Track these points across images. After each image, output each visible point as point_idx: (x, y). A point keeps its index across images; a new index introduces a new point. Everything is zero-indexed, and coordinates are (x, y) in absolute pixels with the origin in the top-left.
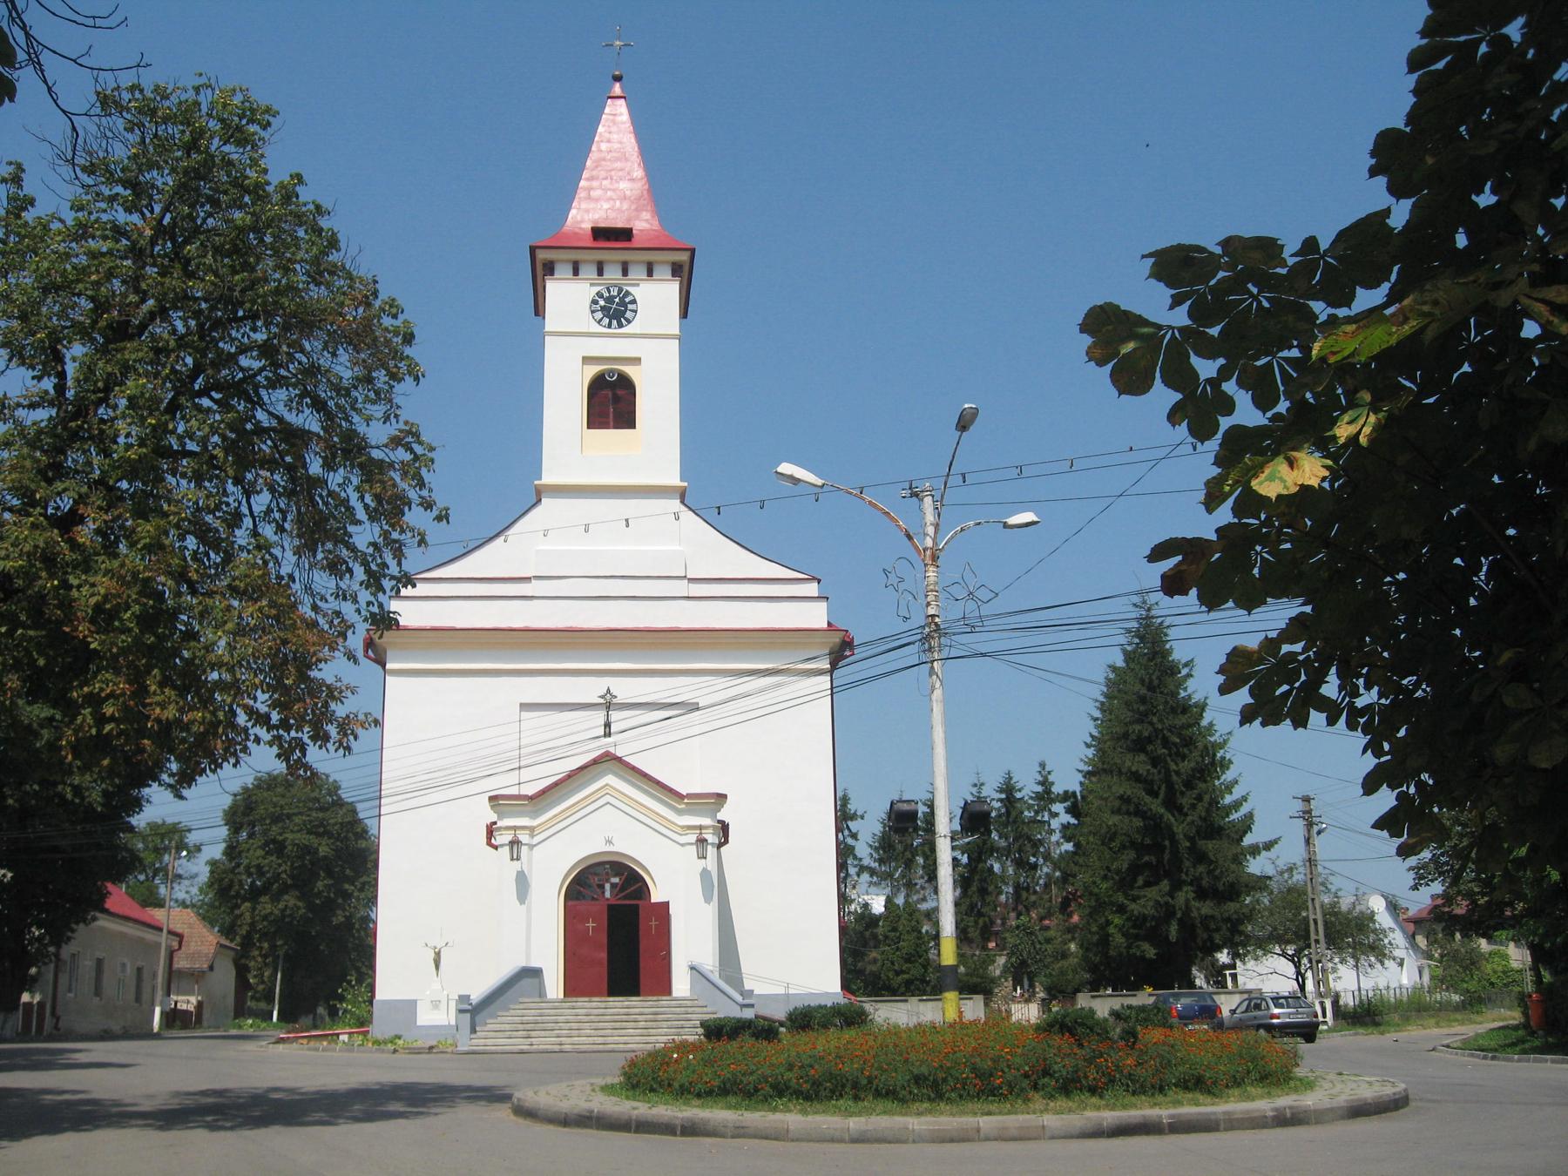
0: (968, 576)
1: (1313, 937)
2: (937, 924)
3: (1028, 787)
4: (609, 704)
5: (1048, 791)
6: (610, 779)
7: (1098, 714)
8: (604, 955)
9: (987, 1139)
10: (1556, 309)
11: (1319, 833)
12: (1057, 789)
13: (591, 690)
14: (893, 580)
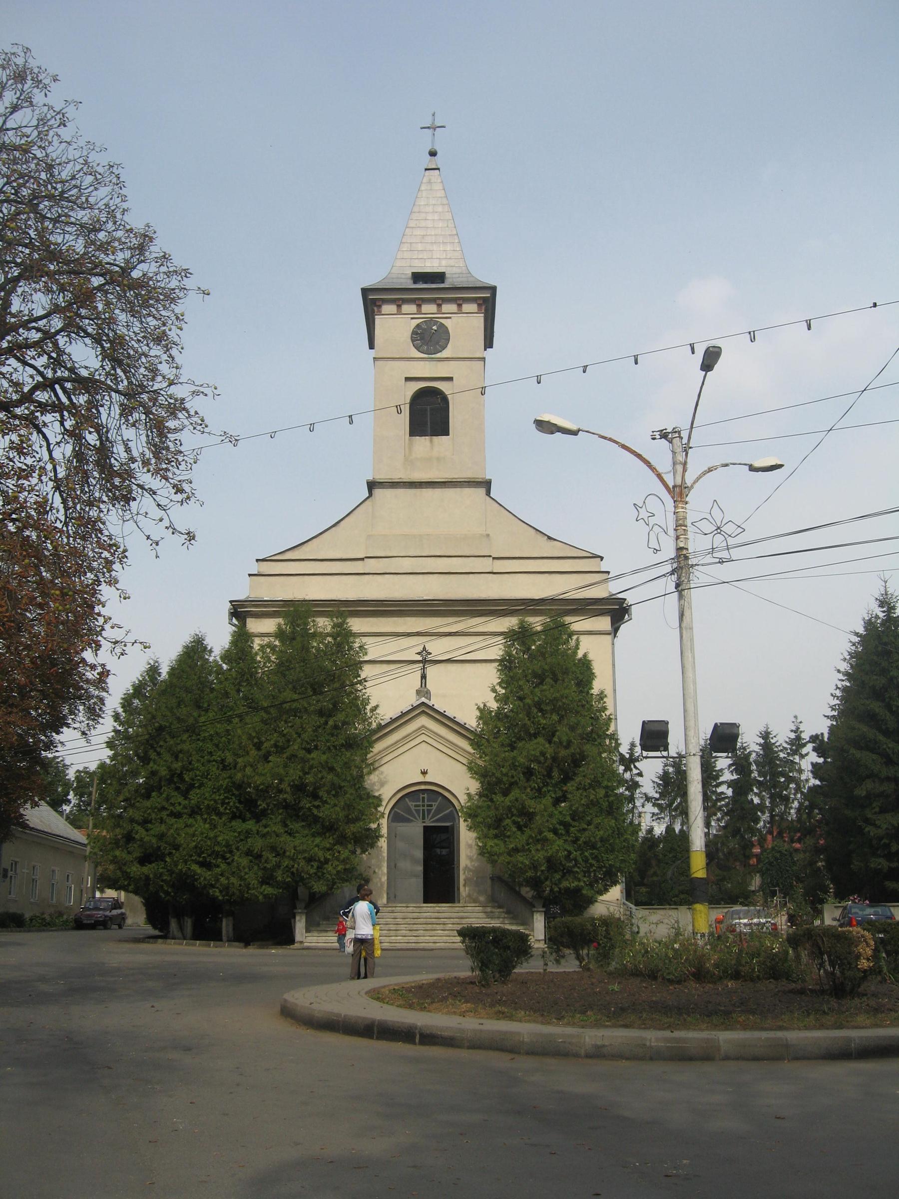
3: (782, 737)
4: (425, 661)
5: (798, 738)
6: (423, 721)
7: (838, 693)
8: (420, 868)
9: (727, 1058)
12: (806, 736)
13: (409, 649)
14: (643, 514)
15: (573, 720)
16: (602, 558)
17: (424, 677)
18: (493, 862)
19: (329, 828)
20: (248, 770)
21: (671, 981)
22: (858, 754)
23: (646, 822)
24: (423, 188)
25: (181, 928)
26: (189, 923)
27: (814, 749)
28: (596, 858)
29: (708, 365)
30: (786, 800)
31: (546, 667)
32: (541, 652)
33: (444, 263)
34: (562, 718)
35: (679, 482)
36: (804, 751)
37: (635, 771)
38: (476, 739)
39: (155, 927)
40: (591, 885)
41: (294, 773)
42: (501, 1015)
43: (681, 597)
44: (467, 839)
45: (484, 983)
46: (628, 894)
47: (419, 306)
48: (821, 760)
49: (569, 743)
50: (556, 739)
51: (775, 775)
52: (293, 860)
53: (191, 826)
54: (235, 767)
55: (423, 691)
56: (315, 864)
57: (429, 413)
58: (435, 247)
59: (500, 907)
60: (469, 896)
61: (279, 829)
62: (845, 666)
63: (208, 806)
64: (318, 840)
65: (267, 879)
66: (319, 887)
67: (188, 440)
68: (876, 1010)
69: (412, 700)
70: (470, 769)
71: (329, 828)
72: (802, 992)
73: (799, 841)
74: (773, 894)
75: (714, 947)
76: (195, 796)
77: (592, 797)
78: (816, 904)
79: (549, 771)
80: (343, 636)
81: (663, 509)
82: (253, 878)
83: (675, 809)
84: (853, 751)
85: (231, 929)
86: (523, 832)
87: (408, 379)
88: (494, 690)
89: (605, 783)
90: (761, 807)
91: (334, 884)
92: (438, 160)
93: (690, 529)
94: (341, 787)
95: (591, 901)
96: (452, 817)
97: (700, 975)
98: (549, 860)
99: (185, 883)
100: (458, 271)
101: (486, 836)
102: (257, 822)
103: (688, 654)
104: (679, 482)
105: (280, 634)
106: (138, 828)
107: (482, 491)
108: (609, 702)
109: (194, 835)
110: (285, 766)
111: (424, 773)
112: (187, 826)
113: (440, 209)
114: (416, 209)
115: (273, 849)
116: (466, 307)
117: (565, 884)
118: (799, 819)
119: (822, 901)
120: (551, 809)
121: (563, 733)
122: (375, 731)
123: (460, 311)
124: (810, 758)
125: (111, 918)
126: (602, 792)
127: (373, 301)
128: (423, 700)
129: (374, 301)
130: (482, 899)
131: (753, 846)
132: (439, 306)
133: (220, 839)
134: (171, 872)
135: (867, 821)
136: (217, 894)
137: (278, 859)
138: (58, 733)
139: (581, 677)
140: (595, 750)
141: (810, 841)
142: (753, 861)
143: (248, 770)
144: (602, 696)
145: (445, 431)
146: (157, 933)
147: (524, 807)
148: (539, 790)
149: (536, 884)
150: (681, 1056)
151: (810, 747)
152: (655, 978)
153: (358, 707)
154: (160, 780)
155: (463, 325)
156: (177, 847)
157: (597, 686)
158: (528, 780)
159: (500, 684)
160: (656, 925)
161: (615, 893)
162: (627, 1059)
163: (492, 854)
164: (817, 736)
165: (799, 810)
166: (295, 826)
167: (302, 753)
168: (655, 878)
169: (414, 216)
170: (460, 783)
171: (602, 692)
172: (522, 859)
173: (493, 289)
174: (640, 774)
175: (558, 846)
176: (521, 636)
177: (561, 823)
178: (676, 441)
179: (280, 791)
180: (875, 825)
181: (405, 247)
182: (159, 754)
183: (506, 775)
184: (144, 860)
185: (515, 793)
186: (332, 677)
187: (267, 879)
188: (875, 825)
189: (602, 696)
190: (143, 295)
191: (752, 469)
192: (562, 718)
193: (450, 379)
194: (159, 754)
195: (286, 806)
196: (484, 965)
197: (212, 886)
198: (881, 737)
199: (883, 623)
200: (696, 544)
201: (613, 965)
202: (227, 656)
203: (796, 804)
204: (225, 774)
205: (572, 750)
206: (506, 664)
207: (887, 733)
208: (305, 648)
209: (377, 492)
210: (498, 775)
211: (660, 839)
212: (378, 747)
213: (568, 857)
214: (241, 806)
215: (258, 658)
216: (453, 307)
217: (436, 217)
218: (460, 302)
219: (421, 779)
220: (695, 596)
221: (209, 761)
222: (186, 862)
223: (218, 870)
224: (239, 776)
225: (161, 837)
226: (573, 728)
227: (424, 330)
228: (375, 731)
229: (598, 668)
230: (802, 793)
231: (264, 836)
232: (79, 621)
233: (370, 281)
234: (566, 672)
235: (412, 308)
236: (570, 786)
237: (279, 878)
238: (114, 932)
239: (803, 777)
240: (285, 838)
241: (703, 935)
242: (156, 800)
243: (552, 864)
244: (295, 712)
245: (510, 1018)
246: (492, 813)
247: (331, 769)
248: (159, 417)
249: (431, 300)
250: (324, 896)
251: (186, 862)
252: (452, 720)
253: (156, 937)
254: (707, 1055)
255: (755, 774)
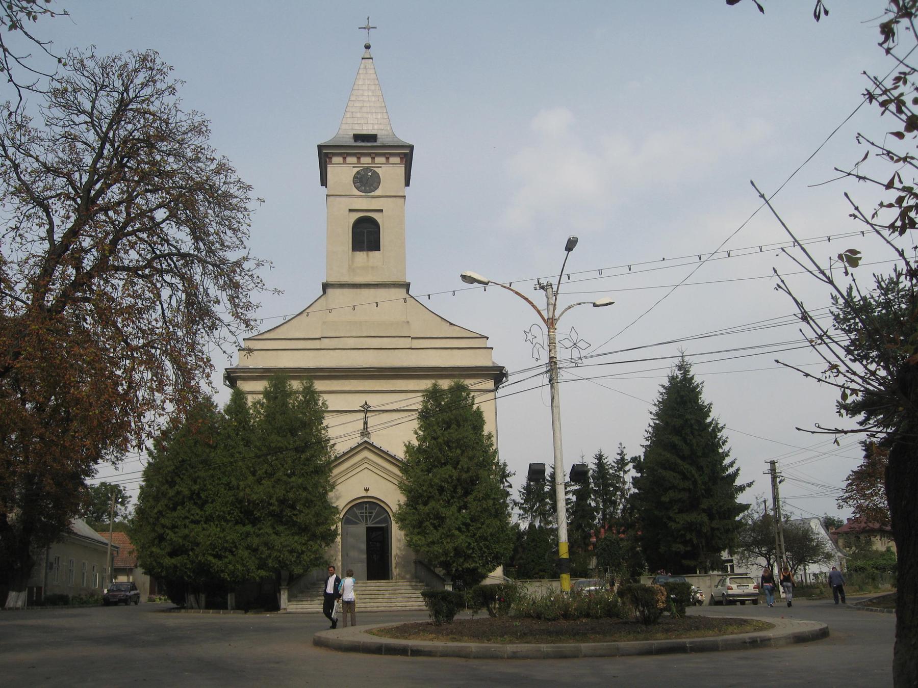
0: (574, 335)
1: (777, 542)
2: (557, 536)
3: (611, 458)
4: (366, 409)
5: (623, 459)
6: (366, 454)
7: (650, 430)
8: (365, 556)
9: (585, 656)
10: (3, 452)
11: (780, 482)
12: (628, 458)
13: (356, 402)
14: (530, 337)
15: (471, 453)
16: (488, 338)
17: (366, 423)
18: (417, 552)
19: (303, 529)
20: (248, 490)
21: (549, 620)
22: (664, 473)
23: (514, 520)
24: (361, 72)
25: (198, 602)
26: (203, 598)
27: (634, 467)
28: (487, 547)
29: (571, 245)
30: (614, 503)
31: (452, 417)
32: (448, 407)
33: (376, 127)
34: (463, 452)
35: (551, 316)
36: (627, 468)
37: (506, 484)
38: (404, 467)
39: (173, 602)
40: (484, 566)
41: (280, 492)
42: (453, 640)
43: (552, 387)
44: (398, 536)
45: (438, 624)
46: (506, 573)
47: (359, 158)
48: (639, 475)
49: (468, 470)
50: (459, 466)
51: (606, 486)
52: (280, 551)
53: (207, 530)
54: (238, 488)
55: (365, 432)
56: (295, 555)
57: (366, 234)
58: (369, 116)
59: (420, 582)
60: (399, 574)
61: (270, 530)
62: (654, 409)
63: (219, 516)
64: (296, 538)
65: (262, 565)
66: (298, 570)
67: (255, 296)
68: (667, 631)
69: (358, 440)
70: (400, 488)
71: (303, 529)
72: (626, 623)
73: (623, 532)
74: (606, 570)
75: (574, 598)
76: (209, 509)
77: (484, 506)
78: (635, 574)
79: (455, 488)
80: (311, 395)
81: (541, 333)
82: (252, 564)
83: (535, 511)
84: (660, 471)
85: (234, 601)
86: (437, 530)
87: (350, 210)
88: (416, 433)
89: (493, 496)
90: (596, 509)
91: (308, 567)
92: (362, 38)
93: (558, 345)
94: (312, 501)
95: (484, 576)
96: (387, 520)
97: (566, 616)
98: (455, 549)
99: (203, 569)
100: (386, 133)
101: (412, 533)
102: (253, 526)
103: (557, 423)
104: (551, 316)
105: (266, 394)
106: (168, 531)
107: (404, 290)
108: (494, 439)
109: (209, 536)
110: (273, 487)
111: (367, 490)
112: (204, 529)
113: (373, 87)
114: (356, 87)
115: (266, 544)
116: (392, 160)
117: (466, 565)
118: (623, 517)
119: (640, 574)
120: (457, 514)
121: (464, 462)
122: (333, 461)
123: (388, 163)
124: (631, 474)
125: (130, 597)
126: (491, 502)
127: (326, 154)
128: (366, 439)
129: (327, 154)
130: (408, 576)
131: (591, 536)
132: (373, 158)
133: (228, 538)
134: (192, 562)
135: (670, 518)
136: (226, 576)
137: (269, 552)
138: (97, 463)
139: (476, 423)
140: (486, 473)
141: (631, 532)
142: (591, 548)
143: (248, 490)
144: (490, 436)
145: (378, 248)
146: (175, 606)
147: (438, 513)
148: (448, 502)
149: (446, 565)
150: (562, 656)
151: (631, 465)
152: (540, 618)
153: (322, 444)
154: (184, 497)
155: (389, 172)
156: (198, 545)
157: (487, 429)
158: (440, 494)
159: (420, 428)
160: (536, 591)
161: (499, 571)
162: (531, 658)
163: (416, 546)
164: (636, 458)
165: (623, 511)
166: (281, 528)
167: (285, 478)
168: (521, 561)
169: (355, 92)
170: (393, 497)
171: (490, 434)
172: (437, 549)
173: (411, 148)
174: (510, 486)
175: (462, 540)
176: (433, 394)
177: (464, 524)
178: (549, 290)
179: (271, 504)
180: (675, 521)
181: (348, 115)
182: (182, 479)
183: (426, 491)
184: (172, 554)
185: (432, 504)
186: (305, 425)
187: (262, 565)
188: (675, 521)
189: (490, 436)
190: (221, 200)
191: (595, 305)
192: (463, 452)
193: (381, 211)
194: (182, 479)
195: (272, 514)
196: (437, 613)
197: (223, 571)
198: (679, 461)
199: (681, 381)
200: (562, 355)
201: (512, 613)
202: (228, 410)
203: (621, 506)
204: (230, 493)
205: (470, 474)
206: (424, 416)
207: (683, 458)
208: (285, 404)
209: (330, 291)
210: (420, 491)
211: (524, 533)
212: (336, 471)
213: (468, 547)
214: (242, 516)
215: (251, 411)
216: (383, 160)
217: (370, 94)
218: (387, 156)
219: (364, 494)
220: (561, 387)
221: (218, 484)
222: (204, 555)
223: (226, 560)
224: (241, 494)
225: (185, 537)
226: (471, 459)
227: (363, 176)
228: (333, 461)
229: (488, 416)
230: (626, 498)
231: (258, 536)
232: (691, 571)
233: (323, 141)
234: (466, 420)
235: (354, 160)
236: (470, 498)
237: (270, 565)
238: (132, 606)
239: (626, 487)
240: (274, 537)
241: (567, 593)
242: (181, 512)
243: (458, 552)
244: (281, 450)
245: (460, 641)
246: (417, 517)
247: (305, 489)
248: (229, 275)
249: (367, 155)
250: (299, 576)
251: (204, 555)
252: (386, 453)
253: (170, 610)
254: (574, 655)
255: (592, 485)
